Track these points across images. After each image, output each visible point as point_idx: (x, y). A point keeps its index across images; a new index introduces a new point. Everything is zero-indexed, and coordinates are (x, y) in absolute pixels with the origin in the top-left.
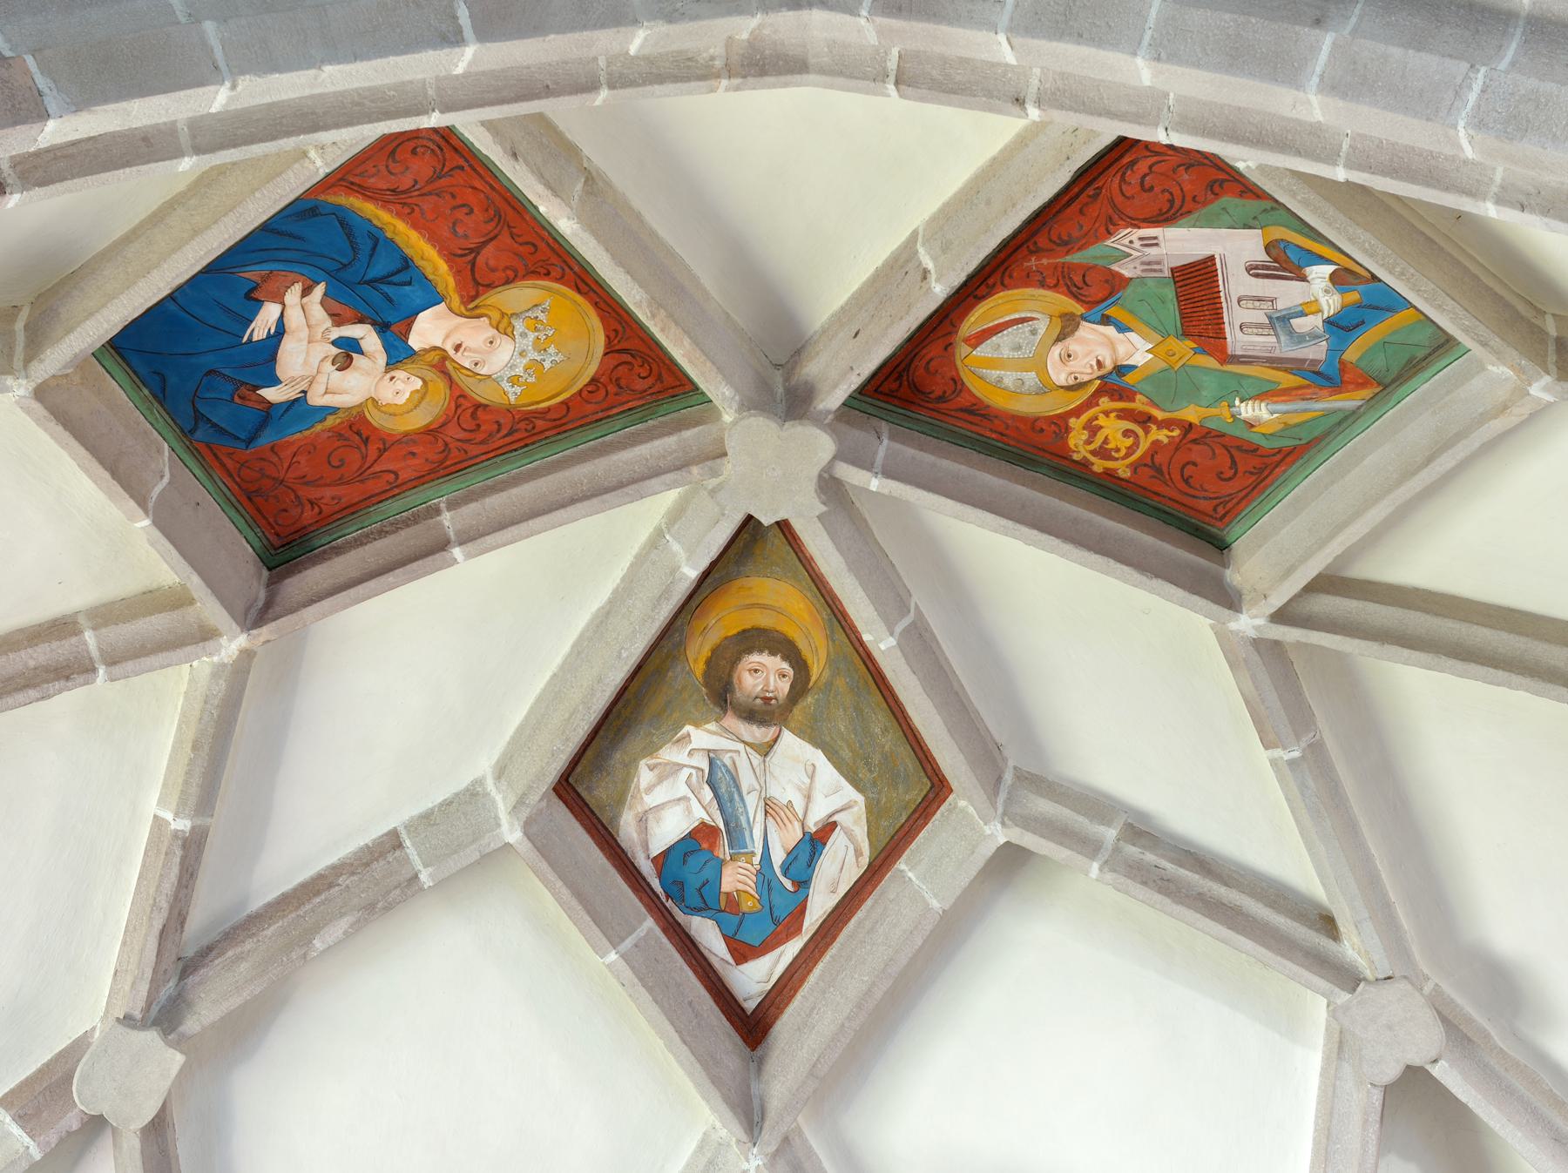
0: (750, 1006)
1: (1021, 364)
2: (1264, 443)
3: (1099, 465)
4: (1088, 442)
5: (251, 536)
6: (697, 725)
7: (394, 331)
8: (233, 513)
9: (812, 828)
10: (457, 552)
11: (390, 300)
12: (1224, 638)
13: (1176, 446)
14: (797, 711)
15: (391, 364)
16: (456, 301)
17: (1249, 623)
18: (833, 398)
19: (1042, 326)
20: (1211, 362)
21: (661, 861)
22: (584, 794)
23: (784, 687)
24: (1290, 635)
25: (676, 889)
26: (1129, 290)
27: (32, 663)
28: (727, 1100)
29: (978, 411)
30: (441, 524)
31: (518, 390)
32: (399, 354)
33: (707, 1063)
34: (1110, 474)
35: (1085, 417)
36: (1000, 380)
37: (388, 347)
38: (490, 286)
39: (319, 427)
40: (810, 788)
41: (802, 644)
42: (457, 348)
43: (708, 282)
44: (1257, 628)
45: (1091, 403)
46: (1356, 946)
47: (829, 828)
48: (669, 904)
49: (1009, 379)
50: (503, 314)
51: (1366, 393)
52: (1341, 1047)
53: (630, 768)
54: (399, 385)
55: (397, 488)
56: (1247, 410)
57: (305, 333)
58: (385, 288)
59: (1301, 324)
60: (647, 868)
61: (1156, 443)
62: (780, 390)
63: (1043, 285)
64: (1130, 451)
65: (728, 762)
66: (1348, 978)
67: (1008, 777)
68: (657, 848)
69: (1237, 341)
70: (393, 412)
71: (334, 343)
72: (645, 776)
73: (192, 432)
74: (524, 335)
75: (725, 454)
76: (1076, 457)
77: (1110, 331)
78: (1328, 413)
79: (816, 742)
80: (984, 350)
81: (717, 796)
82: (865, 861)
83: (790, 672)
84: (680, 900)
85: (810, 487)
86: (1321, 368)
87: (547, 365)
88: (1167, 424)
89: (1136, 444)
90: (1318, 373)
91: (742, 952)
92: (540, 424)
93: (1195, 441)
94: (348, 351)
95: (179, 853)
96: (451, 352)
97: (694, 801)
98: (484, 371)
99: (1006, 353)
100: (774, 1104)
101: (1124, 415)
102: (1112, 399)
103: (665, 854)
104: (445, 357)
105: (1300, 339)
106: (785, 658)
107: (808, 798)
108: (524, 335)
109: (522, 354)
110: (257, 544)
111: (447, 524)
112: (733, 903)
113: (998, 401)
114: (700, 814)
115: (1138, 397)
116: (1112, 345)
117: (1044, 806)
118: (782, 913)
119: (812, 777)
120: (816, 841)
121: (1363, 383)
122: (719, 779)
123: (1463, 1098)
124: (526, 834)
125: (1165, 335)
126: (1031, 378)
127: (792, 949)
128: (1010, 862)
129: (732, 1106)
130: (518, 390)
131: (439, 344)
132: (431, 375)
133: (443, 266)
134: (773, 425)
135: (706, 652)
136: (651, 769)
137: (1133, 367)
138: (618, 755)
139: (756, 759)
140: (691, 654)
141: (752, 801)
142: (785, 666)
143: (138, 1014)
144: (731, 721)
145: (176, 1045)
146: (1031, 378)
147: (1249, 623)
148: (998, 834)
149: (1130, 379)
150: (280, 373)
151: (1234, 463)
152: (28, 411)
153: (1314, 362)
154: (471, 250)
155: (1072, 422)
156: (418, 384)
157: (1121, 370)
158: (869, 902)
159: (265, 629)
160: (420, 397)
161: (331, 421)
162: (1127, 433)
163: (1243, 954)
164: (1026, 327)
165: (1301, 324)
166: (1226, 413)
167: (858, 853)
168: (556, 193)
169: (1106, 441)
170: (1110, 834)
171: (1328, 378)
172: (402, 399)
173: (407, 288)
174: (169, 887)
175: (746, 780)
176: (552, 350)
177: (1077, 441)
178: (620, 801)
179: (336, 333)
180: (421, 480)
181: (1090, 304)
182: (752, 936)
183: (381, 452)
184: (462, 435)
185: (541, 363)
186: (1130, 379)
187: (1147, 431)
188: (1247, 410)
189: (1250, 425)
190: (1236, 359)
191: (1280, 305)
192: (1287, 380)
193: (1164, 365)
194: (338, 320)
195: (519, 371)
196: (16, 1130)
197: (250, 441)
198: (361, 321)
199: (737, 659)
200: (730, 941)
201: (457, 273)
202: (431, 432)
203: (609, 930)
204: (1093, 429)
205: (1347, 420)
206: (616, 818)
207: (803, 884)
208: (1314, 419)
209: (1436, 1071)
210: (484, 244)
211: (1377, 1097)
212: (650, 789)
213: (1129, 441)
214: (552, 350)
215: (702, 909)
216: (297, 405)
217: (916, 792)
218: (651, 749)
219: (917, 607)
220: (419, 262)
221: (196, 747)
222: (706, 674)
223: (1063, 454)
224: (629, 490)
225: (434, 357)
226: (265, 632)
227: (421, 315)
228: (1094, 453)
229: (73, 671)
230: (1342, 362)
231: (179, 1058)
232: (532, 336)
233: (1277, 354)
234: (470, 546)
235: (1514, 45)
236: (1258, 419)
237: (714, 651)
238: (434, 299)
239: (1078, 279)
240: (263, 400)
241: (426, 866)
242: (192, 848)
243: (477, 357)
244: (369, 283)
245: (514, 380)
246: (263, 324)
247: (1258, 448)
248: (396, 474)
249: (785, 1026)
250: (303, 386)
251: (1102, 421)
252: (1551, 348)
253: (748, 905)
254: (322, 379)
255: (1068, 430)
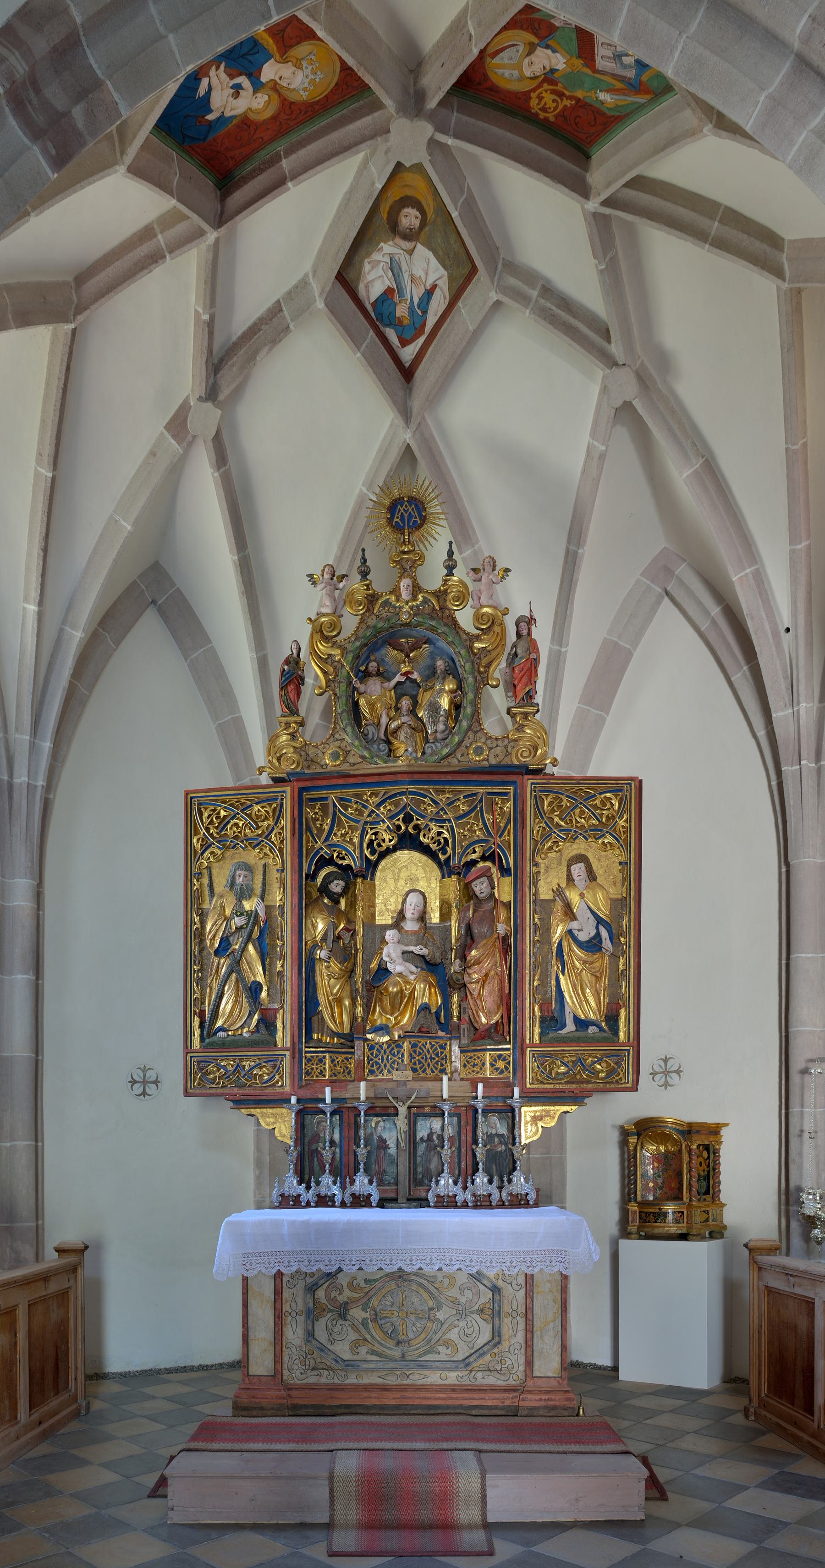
0: (407, 365)
1: (512, 67)
2: (607, 112)
3: (542, 115)
4: (538, 104)
5: (211, 177)
6: (385, 242)
7: (254, 76)
8: (203, 170)
9: (428, 288)
10: (290, 184)
11: (251, 62)
12: (583, 210)
13: (573, 108)
14: (422, 234)
15: (255, 91)
16: (277, 56)
17: (593, 205)
18: (432, 104)
19: (521, 48)
20: (588, 71)
21: (374, 304)
22: (345, 276)
23: (417, 223)
24: (607, 211)
25: (380, 316)
26: (558, 33)
27: (142, 254)
28: (398, 410)
29: (494, 89)
30: (282, 166)
31: (306, 93)
32: (258, 86)
33: (391, 394)
34: (546, 119)
35: (537, 93)
36: (503, 74)
37: (253, 84)
38: (291, 47)
39: (230, 126)
40: (428, 269)
41: (424, 203)
42: (280, 78)
43: (381, 32)
44: (595, 208)
45: (540, 86)
46: (616, 349)
47: (434, 287)
48: (378, 323)
49: (507, 73)
50: (297, 59)
51: (649, 97)
52: (604, 390)
53: (361, 263)
54: (259, 100)
55: (263, 145)
56: (603, 96)
57: (219, 87)
58: (249, 57)
59: (625, 59)
60: (369, 308)
61: (565, 106)
62: (412, 91)
63: (522, 28)
64: (555, 109)
65: (397, 259)
66: (611, 363)
67: (500, 266)
68: (373, 299)
69: (600, 63)
70: (258, 112)
71: (232, 88)
72: (367, 267)
73: (183, 143)
74: (307, 68)
75: (388, 131)
76: (533, 111)
77: (549, 52)
78: (633, 103)
79: (430, 248)
80: (496, 60)
81: (393, 274)
82: (447, 301)
83: (419, 216)
84: (382, 321)
85: (424, 148)
86: (632, 82)
87: (317, 80)
88: (570, 98)
89: (557, 106)
90: (630, 84)
91: (404, 343)
92: (317, 107)
93: (581, 107)
94: (237, 88)
95: (207, 329)
96: (278, 81)
97: (385, 278)
98: (292, 87)
99: (506, 61)
100: (415, 411)
101: (554, 92)
102: (549, 85)
103: (375, 301)
104: (276, 83)
105: (625, 67)
106: (418, 210)
107: (427, 274)
108: (307, 68)
109: (307, 77)
110: (214, 180)
111: (285, 166)
112: (400, 321)
113: (502, 84)
114: (388, 283)
115: (559, 84)
116: (549, 58)
117: (512, 281)
118: (418, 325)
119: (428, 264)
120: (429, 293)
121: (647, 92)
122: (394, 267)
123: (641, 413)
124: (326, 304)
125: (572, 57)
126: (516, 73)
127: (421, 340)
128: (498, 304)
129: (401, 413)
130: (306, 93)
131: (273, 78)
132: (271, 93)
133: (271, 41)
134: (409, 122)
135: (387, 209)
136: (369, 263)
137: (557, 70)
138: (356, 258)
139: (408, 257)
140: (382, 210)
141: (406, 277)
142: (418, 213)
143: (204, 396)
144: (398, 240)
145: (216, 406)
146: (516, 73)
147: (593, 205)
148: (494, 296)
149: (556, 75)
150: (212, 107)
151: (595, 120)
152: (126, 177)
153: (630, 79)
154: (281, 31)
155: (532, 94)
156: (267, 97)
157: (553, 71)
158: (448, 320)
159: (223, 228)
160: (269, 102)
161: (235, 122)
162: (554, 101)
163: (577, 350)
164: (514, 49)
165: (626, 60)
166: (593, 96)
167: (445, 298)
168: (316, 20)
169: (545, 104)
170: (534, 293)
171: (634, 87)
172: (261, 106)
173: (257, 55)
174: (205, 344)
175: (404, 267)
176: (319, 73)
177: (534, 103)
178: (358, 279)
179: (232, 83)
180: (273, 140)
181: (541, 38)
182: (407, 336)
183: (255, 130)
184: (286, 117)
185: (314, 80)
186: (556, 75)
187: (562, 100)
188: (603, 96)
189: (602, 103)
190: (599, 72)
191: (619, 49)
192: (619, 85)
193: (570, 70)
194: (232, 77)
195: (306, 85)
196: (173, 442)
197: (205, 139)
198: (241, 75)
199: (400, 211)
200: (400, 338)
201: (277, 42)
202: (274, 118)
203: (355, 340)
204: (540, 98)
205: (639, 108)
206: (357, 286)
207: (425, 312)
208: (628, 105)
209: (634, 403)
210: (286, 27)
211: (613, 411)
212: (369, 273)
213: (555, 105)
214: (319, 73)
215: (389, 325)
216: (221, 119)
217: (466, 271)
218: (369, 255)
219: (469, 187)
220: (261, 41)
221: (206, 283)
222: (388, 219)
223: (528, 109)
224: (354, 149)
225: (271, 84)
226: (223, 230)
227: (265, 66)
228: (540, 109)
229: (156, 258)
230: (640, 81)
231: (219, 412)
232: (310, 68)
233: (615, 72)
234: (295, 181)
235: (700, 15)
236: (606, 101)
237: (391, 208)
238: (269, 57)
239: (536, 26)
240: (208, 120)
241: (292, 321)
242: (210, 325)
243: (289, 81)
244: (242, 56)
245: (304, 90)
246: (202, 90)
247: (605, 114)
248: (262, 138)
249: (419, 373)
250: (222, 110)
251: (544, 94)
252: (715, 116)
253: (406, 322)
254: (229, 105)
255: (530, 98)
